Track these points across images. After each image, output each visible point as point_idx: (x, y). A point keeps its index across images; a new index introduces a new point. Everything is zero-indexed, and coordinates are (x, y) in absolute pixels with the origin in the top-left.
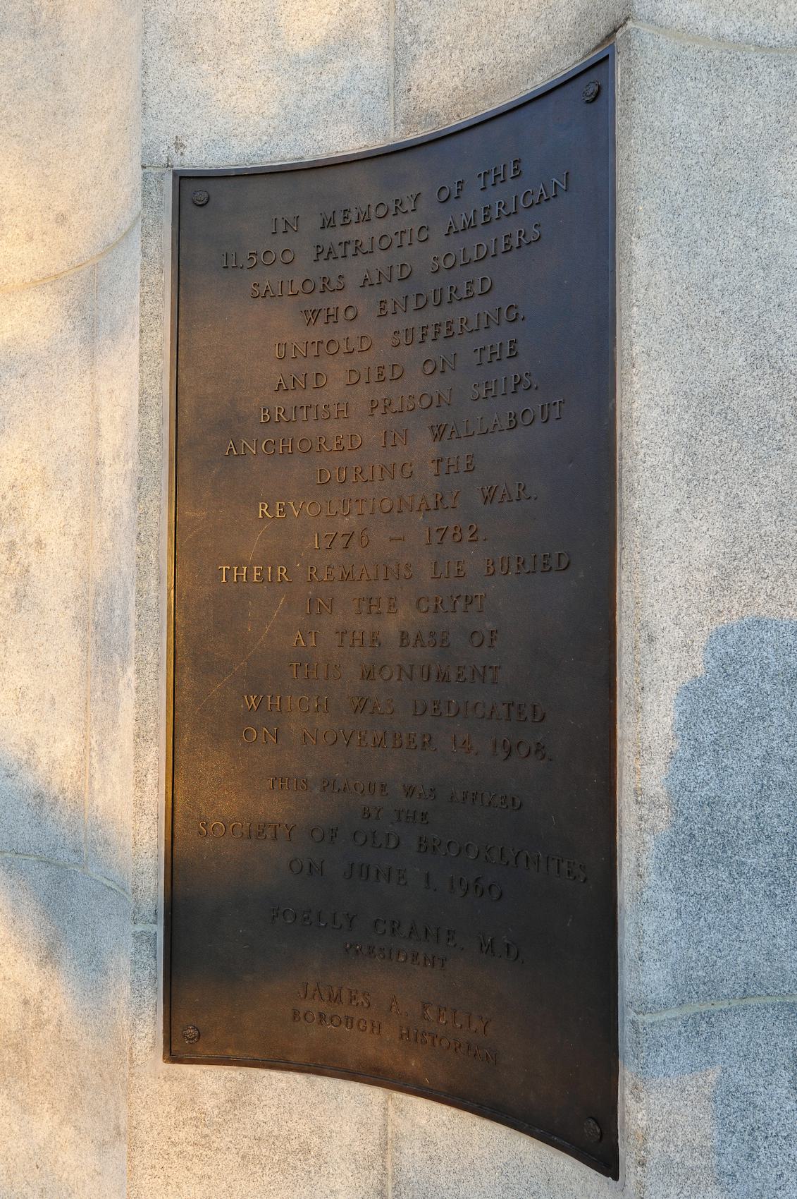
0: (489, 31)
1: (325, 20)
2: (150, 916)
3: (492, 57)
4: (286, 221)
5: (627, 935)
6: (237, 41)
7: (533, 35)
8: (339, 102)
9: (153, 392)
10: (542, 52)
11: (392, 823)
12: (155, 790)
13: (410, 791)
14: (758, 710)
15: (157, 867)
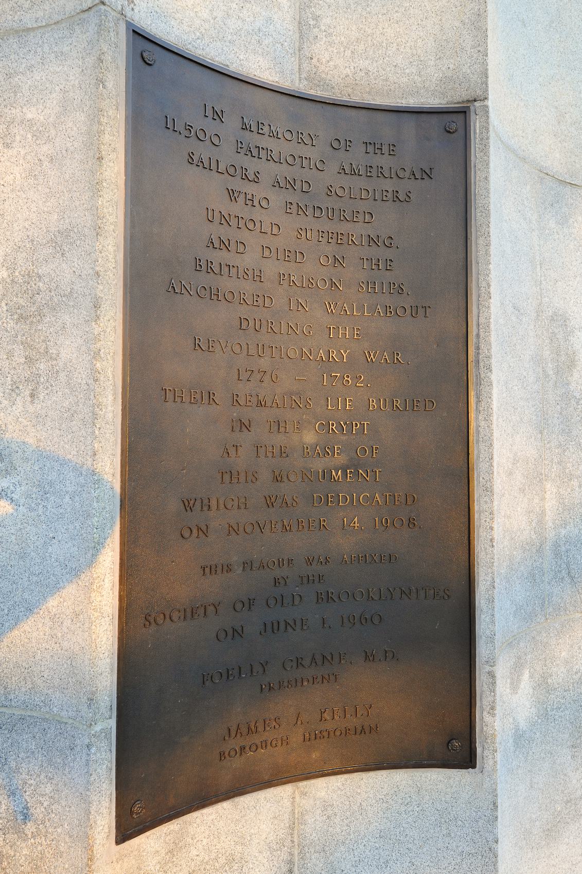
2: (107, 712)
7: (407, 71)
10: (414, 85)
15: (112, 665)
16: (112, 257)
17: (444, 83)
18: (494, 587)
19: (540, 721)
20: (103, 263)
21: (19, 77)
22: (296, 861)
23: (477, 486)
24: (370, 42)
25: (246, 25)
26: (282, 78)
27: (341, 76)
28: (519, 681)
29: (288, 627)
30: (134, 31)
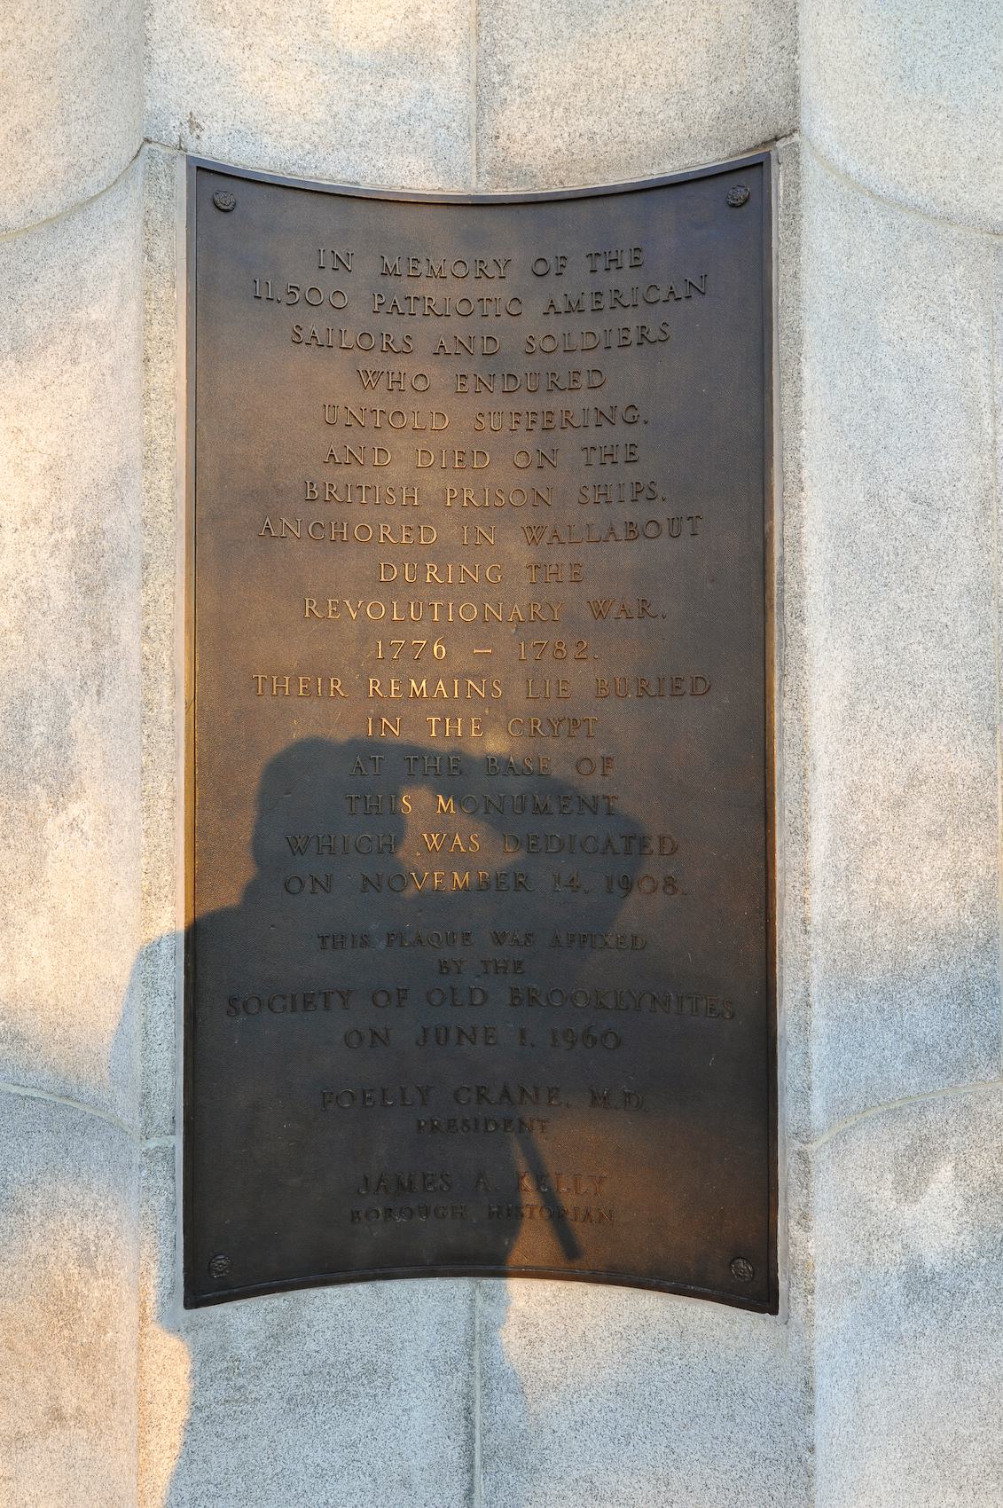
0: (603, 97)
1: (387, 23)
2: (166, 1125)
3: (606, 128)
4: (690, 283)
5: (790, 1066)
6: (270, 13)
7: (661, 117)
8: (406, 128)
9: (165, 443)
10: (672, 138)
11: (478, 976)
12: (171, 962)
13: (499, 939)
14: (872, 835)
16: (166, 496)
17: (725, 121)
18: (809, 1005)
19: (983, 1261)
20: (151, 505)
21: (84, 267)
22: (478, 1397)
23: (781, 824)
24: (596, 84)
25: (388, 112)
26: (448, 181)
27: (548, 155)
28: (922, 1180)
29: (464, 1040)
30: (198, 168)
